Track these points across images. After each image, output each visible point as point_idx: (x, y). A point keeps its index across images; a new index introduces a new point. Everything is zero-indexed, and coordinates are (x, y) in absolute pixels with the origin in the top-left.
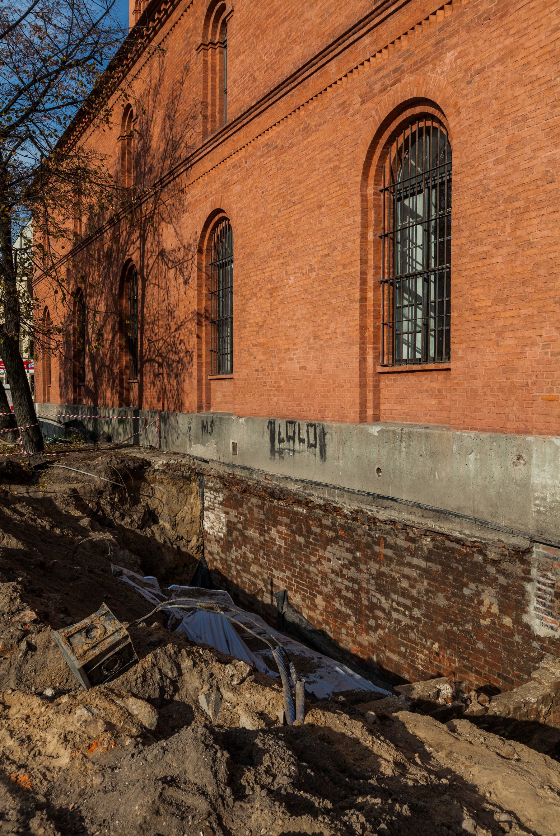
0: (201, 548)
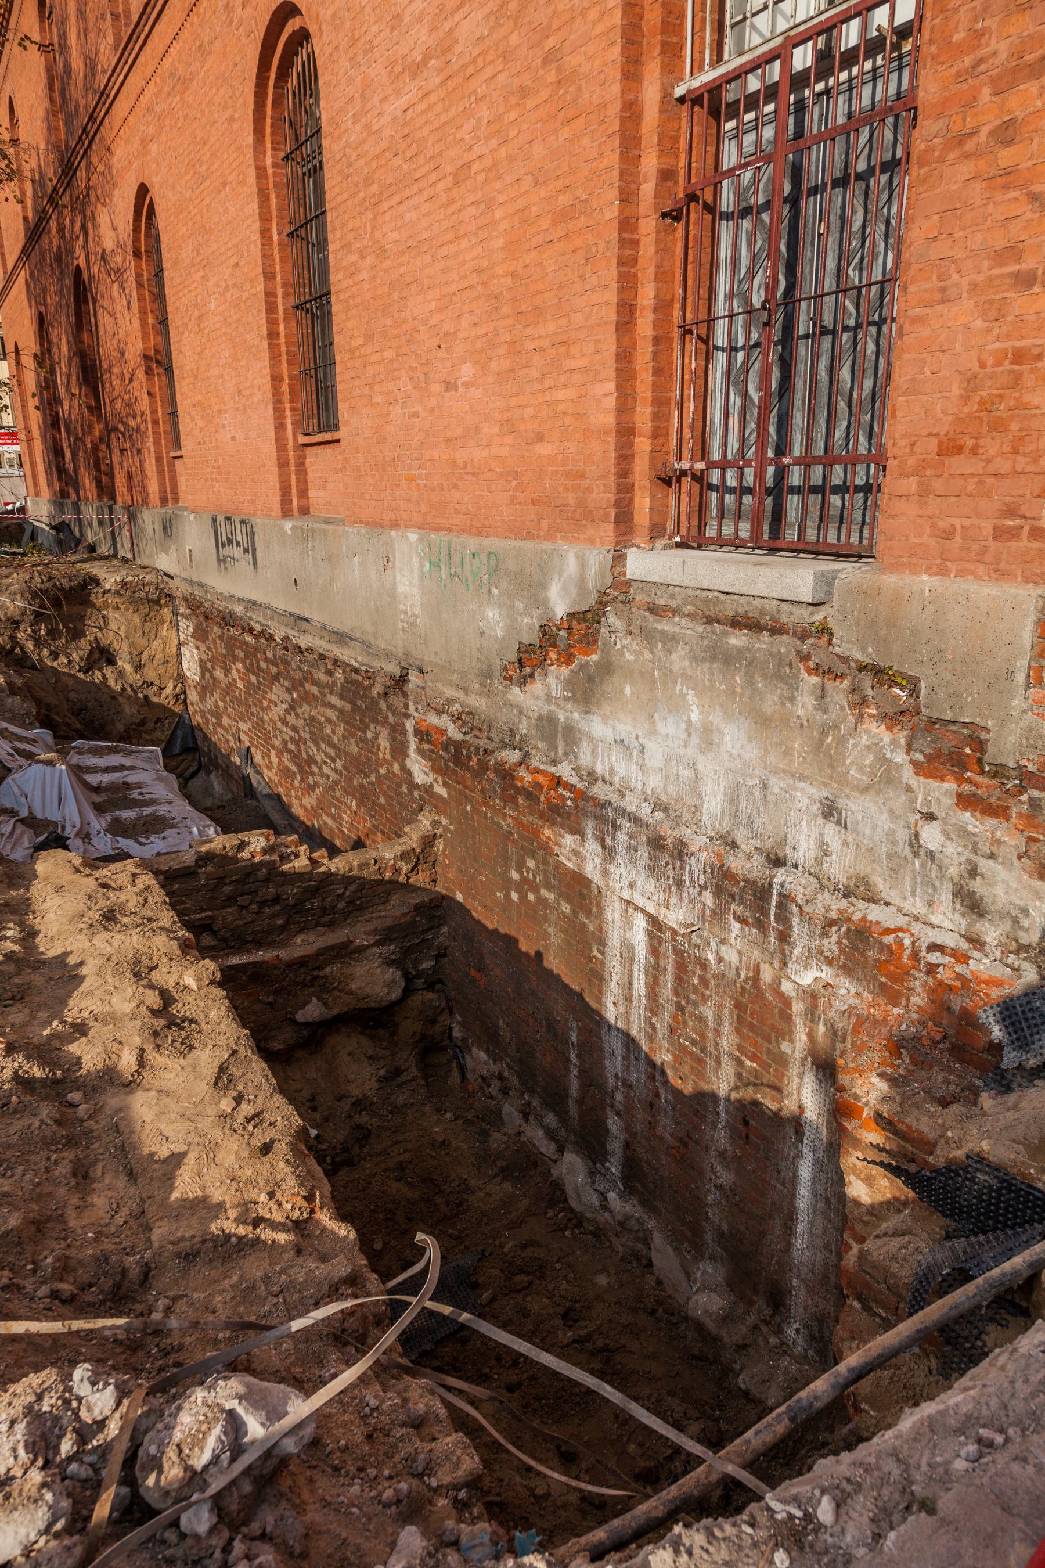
0: (181, 697)
